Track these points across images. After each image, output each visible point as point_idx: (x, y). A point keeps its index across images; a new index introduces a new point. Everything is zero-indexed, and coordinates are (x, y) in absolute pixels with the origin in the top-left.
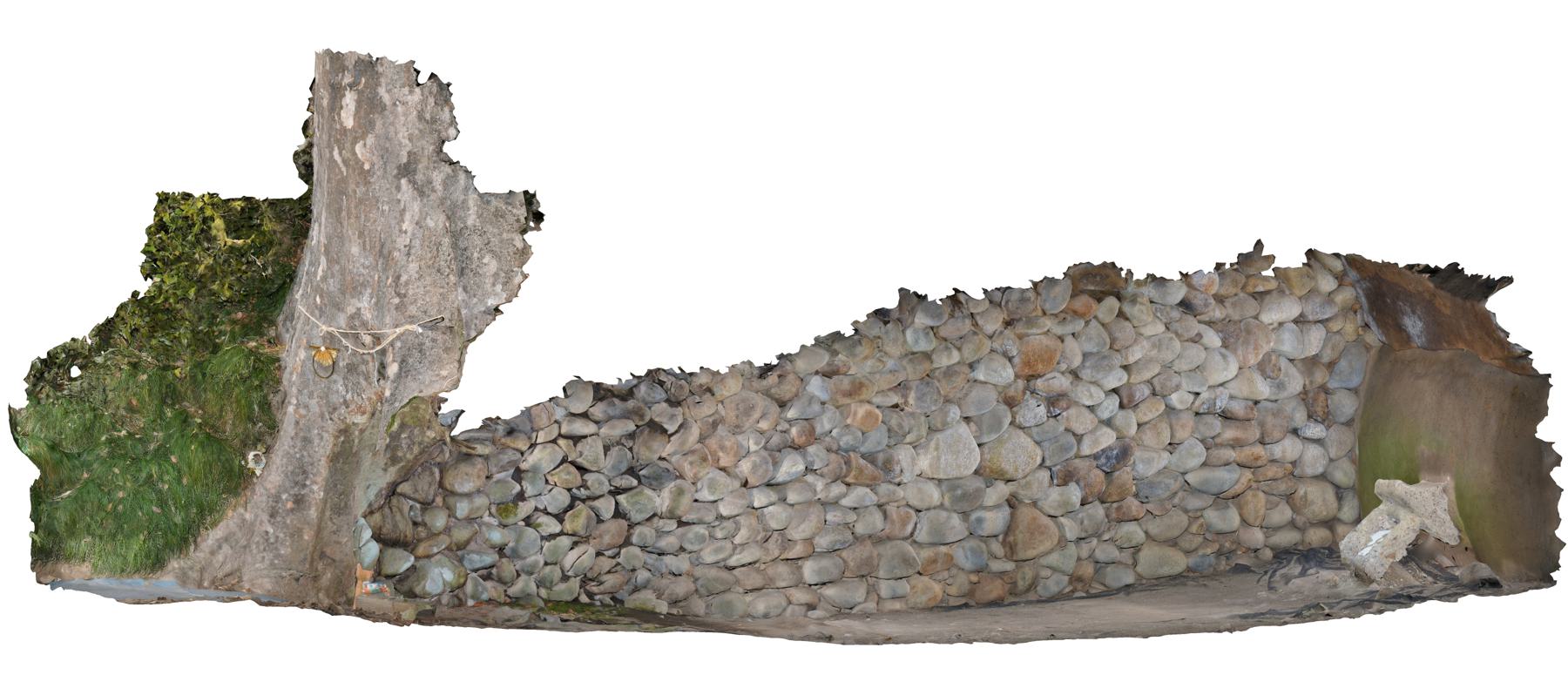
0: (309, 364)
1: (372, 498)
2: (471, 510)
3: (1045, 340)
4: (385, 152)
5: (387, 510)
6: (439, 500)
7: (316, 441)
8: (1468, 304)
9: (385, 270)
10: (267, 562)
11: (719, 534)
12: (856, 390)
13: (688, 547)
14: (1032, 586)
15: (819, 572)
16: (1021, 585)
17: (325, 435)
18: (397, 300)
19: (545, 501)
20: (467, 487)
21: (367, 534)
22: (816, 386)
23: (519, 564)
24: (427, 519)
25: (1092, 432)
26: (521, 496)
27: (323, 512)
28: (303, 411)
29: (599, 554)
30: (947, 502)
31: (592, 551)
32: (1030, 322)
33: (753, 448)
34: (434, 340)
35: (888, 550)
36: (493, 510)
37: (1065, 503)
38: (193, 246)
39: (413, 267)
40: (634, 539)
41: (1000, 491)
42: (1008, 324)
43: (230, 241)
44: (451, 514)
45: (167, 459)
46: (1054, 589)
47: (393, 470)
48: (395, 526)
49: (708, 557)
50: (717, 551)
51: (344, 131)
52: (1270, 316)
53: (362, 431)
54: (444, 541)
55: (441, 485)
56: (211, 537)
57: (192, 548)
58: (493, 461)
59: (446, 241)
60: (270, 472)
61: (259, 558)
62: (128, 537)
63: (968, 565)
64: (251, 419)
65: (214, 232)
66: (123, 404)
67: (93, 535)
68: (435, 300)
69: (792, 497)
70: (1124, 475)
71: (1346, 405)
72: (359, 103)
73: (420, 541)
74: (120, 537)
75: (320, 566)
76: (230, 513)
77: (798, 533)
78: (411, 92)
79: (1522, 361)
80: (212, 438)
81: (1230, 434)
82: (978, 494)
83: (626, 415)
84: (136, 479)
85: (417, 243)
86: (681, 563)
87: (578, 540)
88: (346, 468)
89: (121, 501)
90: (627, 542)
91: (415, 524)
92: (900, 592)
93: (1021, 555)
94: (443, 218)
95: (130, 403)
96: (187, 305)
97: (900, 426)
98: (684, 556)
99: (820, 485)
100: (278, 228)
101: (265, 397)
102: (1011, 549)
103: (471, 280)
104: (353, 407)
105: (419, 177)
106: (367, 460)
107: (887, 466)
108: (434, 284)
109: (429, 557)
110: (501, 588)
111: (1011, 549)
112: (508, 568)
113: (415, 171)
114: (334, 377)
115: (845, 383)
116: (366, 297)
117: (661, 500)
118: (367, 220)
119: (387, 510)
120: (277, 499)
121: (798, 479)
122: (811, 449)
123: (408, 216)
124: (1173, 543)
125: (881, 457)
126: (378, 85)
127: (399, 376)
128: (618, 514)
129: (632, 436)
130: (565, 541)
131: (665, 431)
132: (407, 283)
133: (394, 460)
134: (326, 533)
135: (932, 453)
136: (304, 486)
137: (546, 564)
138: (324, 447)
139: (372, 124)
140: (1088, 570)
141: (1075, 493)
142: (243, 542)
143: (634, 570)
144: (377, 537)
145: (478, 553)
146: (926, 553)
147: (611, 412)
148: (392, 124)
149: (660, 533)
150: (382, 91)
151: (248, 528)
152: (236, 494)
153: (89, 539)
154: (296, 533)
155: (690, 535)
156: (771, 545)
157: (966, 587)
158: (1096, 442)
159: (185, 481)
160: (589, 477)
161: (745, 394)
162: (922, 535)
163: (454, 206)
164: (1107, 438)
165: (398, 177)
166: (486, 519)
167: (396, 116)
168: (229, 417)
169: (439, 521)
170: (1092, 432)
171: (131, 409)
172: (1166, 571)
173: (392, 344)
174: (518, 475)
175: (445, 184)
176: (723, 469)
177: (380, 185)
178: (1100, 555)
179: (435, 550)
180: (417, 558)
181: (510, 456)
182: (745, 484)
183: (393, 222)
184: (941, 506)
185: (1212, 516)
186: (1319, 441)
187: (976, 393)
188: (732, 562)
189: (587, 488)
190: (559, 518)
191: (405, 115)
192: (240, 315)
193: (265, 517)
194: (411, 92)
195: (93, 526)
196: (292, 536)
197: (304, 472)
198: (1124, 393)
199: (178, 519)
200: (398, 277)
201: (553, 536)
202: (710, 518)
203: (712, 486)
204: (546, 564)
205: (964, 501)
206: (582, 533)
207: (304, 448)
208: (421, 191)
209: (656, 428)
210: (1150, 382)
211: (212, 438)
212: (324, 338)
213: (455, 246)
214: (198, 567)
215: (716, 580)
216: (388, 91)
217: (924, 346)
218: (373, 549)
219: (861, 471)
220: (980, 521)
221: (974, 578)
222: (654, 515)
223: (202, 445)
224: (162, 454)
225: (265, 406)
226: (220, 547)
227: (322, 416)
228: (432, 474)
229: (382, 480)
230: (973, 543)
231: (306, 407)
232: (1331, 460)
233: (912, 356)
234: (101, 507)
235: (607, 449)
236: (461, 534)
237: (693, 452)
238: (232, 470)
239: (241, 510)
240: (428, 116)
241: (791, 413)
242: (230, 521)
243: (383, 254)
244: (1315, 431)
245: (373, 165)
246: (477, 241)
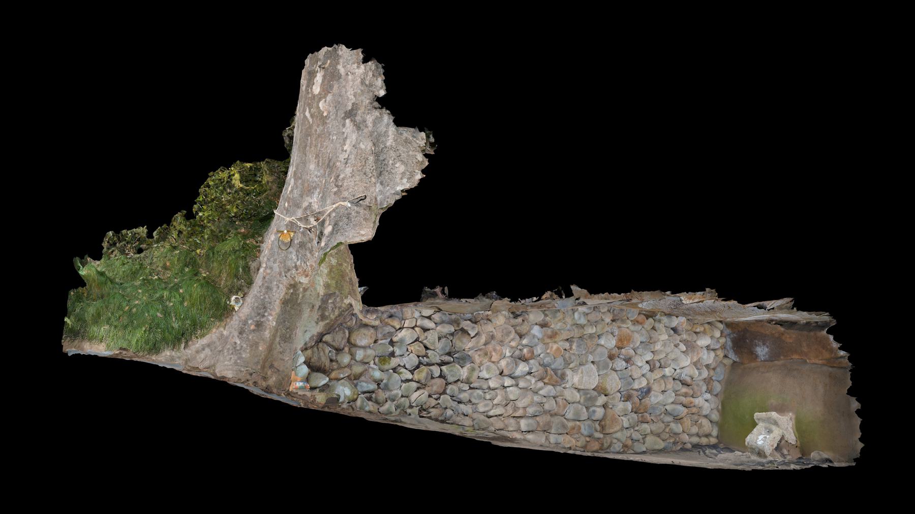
0: (276, 243)
1: (307, 339)
2: (365, 356)
4: (337, 104)
5: (315, 349)
6: (346, 349)
7: (275, 289)
8: (812, 334)
9: (330, 174)
10: (233, 361)
11: (488, 397)
12: (553, 336)
13: (473, 400)
14: (610, 446)
15: (528, 425)
16: (606, 445)
17: (281, 286)
18: (336, 189)
19: (405, 361)
20: (363, 342)
21: (302, 359)
22: (536, 330)
23: (388, 394)
24: (339, 358)
25: (639, 378)
26: (392, 354)
27: (274, 336)
28: (268, 271)
29: (430, 396)
30: (582, 401)
31: (426, 393)
32: (623, 321)
33: (508, 354)
34: (358, 212)
35: (556, 420)
36: (377, 360)
37: (625, 410)
38: (222, 193)
39: (348, 170)
40: (448, 391)
41: (602, 400)
42: (613, 321)
43: (241, 186)
44: (353, 355)
45: (177, 290)
46: (618, 449)
47: (322, 324)
48: (319, 358)
49: (481, 408)
50: (486, 405)
51: (314, 96)
53: (305, 290)
54: (347, 372)
55: (349, 341)
56: (198, 343)
57: (183, 345)
58: (380, 330)
59: (371, 158)
60: (243, 307)
61: (228, 358)
62: (135, 329)
63: (586, 433)
64: (236, 276)
65: (233, 182)
66: (161, 265)
67: (111, 325)
68: (361, 189)
69: (522, 384)
70: (646, 401)
71: (718, 387)
72: (324, 77)
73: (333, 370)
74: (130, 329)
75: (269, 373)
76: (214, 330)
77: (520, 404)
78: (358, 67)
80: (210, 283)
81: (684, 390)
82: (595, 399)
83: (451, 322)
84: (151, 296)
85: (352, 157)
87: (421, 386)
88: (293, 312)
89: (135, 306)
90: (444, 393)
91: (331, 361)
93: (607, 431)
94: (370, 144)
95: (165, 264)
96: (213, 224)
97: (570, 358)
98: (469, 406)
99: (533, 381)
100: (270, 179)
101: (247, 263)
102: (603, 428)
103: (386, 176)
104: (300, 270)
105: (358, 118)
106: (306, 313)
107: (563, 377)
108: (361, 180)
109: (338, 380)
110: (376, 406)
111: (603, 428)
112: (382, 395)
113: (355, 115)
114: (291, 249)
115: (549, 331)
116: (316, 195)
117: (464, 373)
118: (322, 147)
119: (315, 349)
120: (245, 323)
121: (523, 377)
122: (531, 362)
123: (348, 142)
125: (559, 372)
126: (338, 63)
127: (332, 233)
128: (442, 376)
129: (452, 334)
130: (414, 385)
131: (469, 334)
132: (343, 179)
133: (323, 317)
134: (275, 352)
135: (579, 375)
136: (264, 316)
137: (402, 396)
138: (279, 293)
139: (331, 87)
140: (629, 442)
141: (629, 406)
142: (220, 348)
143: (446, 408)
144: (307, 363)
145: (366, 382)
146: (570, 424)
147: (444, 318)
148: (344, 87)
149: (461, 391)
150: (340, 67)
151: (224, 339)
152: (221, 320)
153: (107, 327)
154: (255, 345)
155: (475, 394)
156: (509, 408)
157: (584, 443)
158: (640, 383)
159: (185, 304)
160: (430, 352)
161: (506, 326)
162: (570, 415)
163: (379, 135)
164: (644, 383)
165: (344, 119)
166: (372, 365)
167: (347, 81)
168: (224, 276)
169: (346, 359)
170: (639, 378)
171: (165, 268)
172: (657, 447)
173: (329, 215)
174: (392, 343)
175: (375, 123)
176: (493, 362)
177: (332, 124)
179: (342, 376)
180: (330, 380)
181: (388, 329)
182: (501, 373)
183: (338, 145)
185: (673, 425)
187: (599, 349)
188: (491, 413)
189: (428, 357)
190: (412, 372)
191: (353, 81)
192: (243, 230)
193: (236, 334)
194: (358, 67)
195: (113, 319)
196: (251, 346)
197: (265, 308)
198: (651, 363)
199: (176, 325)
200: (338, 176)
201: (408, 381)
202: (485, 387)
203: (488, 369)
204: (402, 396)
206: (423, 381)
207: (267, 293)
208: (358, 127)
209: (464, 331)
211: (210, 283)
212: (287, 225)
213: (376, 161)
214: (185, 358)
215: (484, 421)
216: (344, 67)
217: (583, 321)
218: (305, 370)
221: (588, 439)
222: (458, 380)
223: (202, 286)
224: (176, 287)
225: (247, 269)
226: (203, 349)
227: (280, 274)
228: (344, 333)
229: (316, 329)
230: (589, 422)
231: (271, 268)
234: (120, 308)
235: (439, 339)
236: (358, 369)
237: (480, 350)
238: (219, 304)
239: (222, 329)
240: (367, 82)
241: (525, 342)
242: (213, 335)
243: (330, 166)
245: (329, 112)
246: (392, 154)
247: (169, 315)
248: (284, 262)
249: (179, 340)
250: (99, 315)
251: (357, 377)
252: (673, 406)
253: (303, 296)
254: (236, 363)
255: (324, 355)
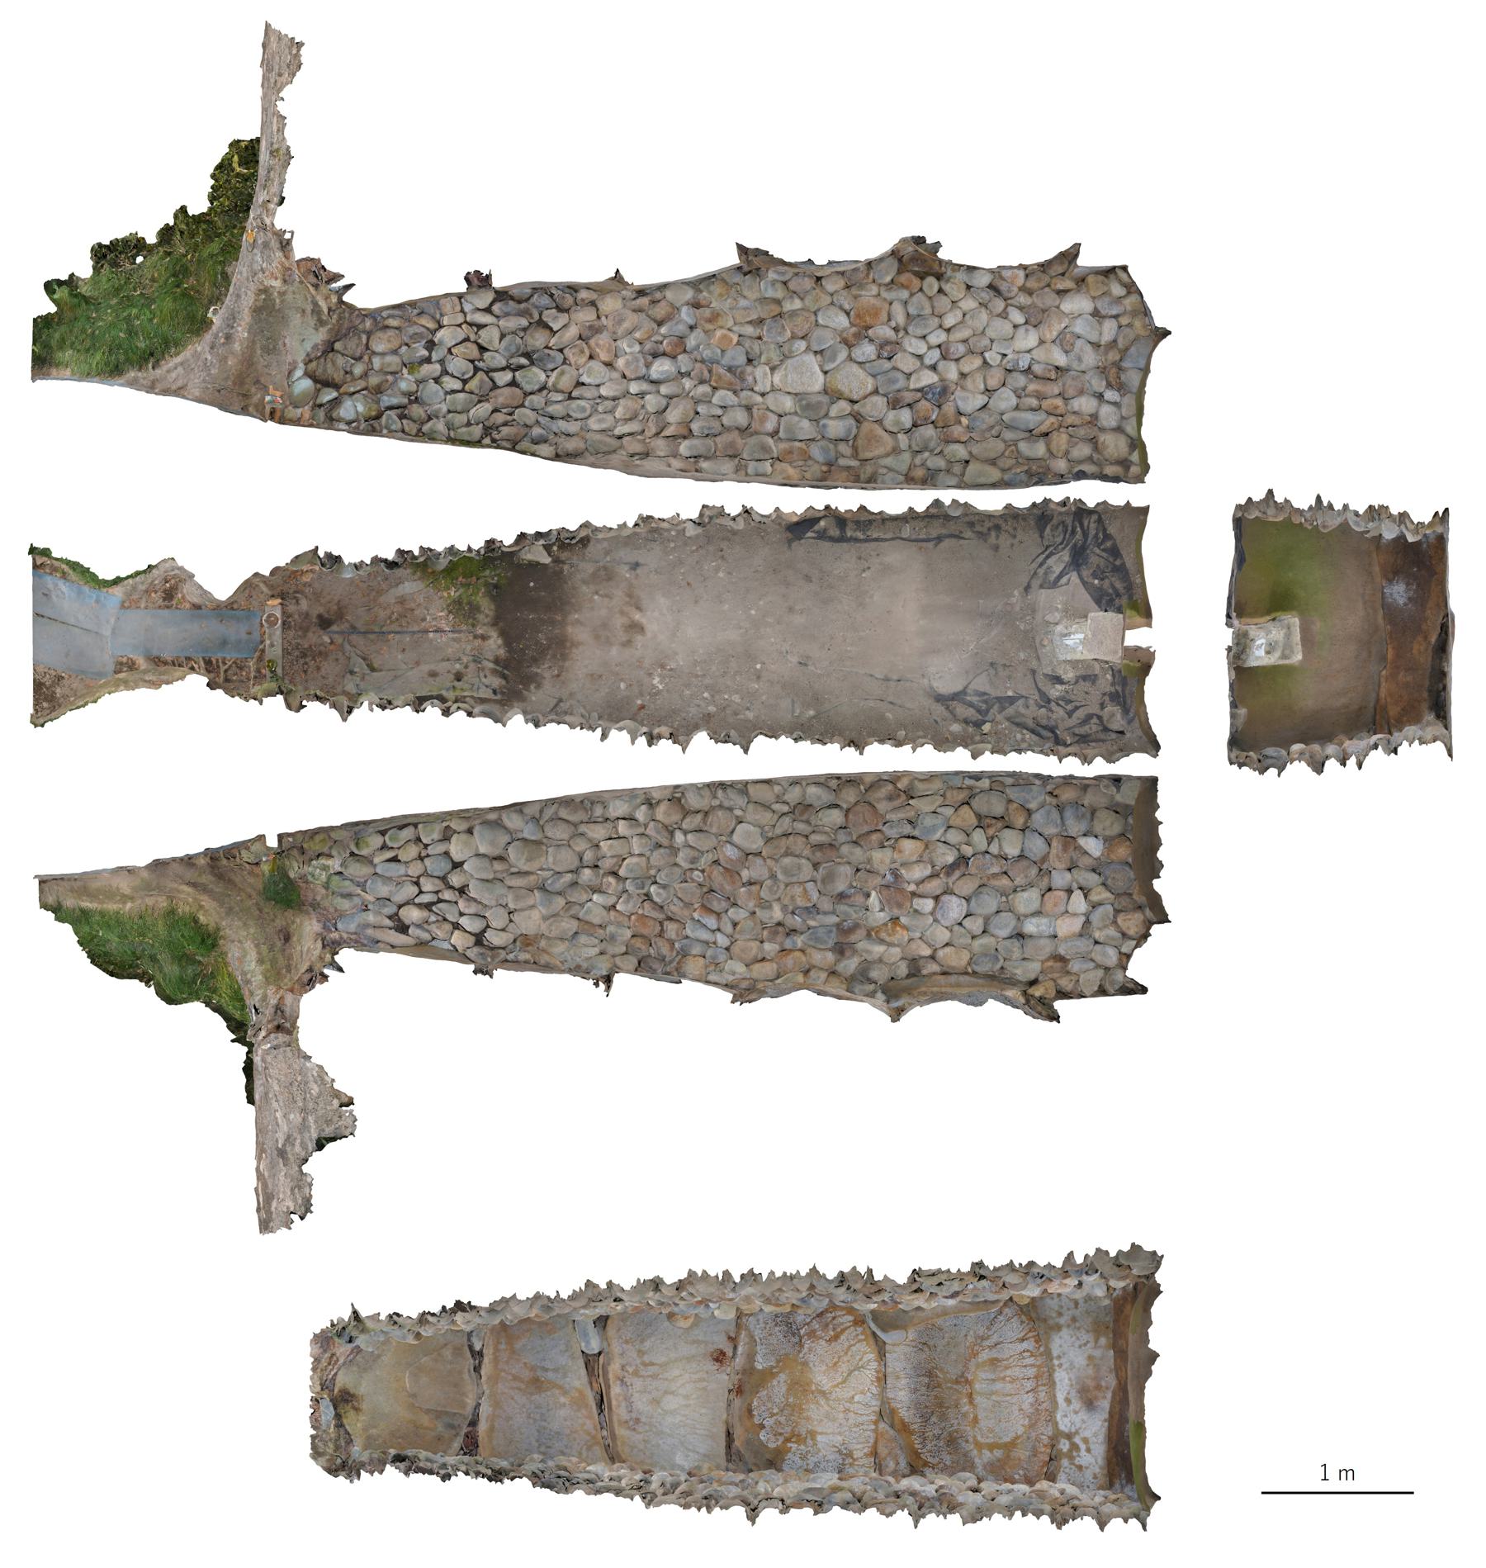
3: (873, 301)
15: (690, 448)
22: (686, 315)
32: (861, 286)
42: (848, 287)
48: (325, 370)
50: (600, 421)
52: (1068, 305)
75: (253, 390)
79: (1148, 1500)
83: (521, 314)
86: (573, 427)
92: (761, 471)
106: (296, 319)
115: (707, 313)
120: (216, 336)
124: (993, 462)
129: (525, 330)
131: (551, 329)
133: (321, 323)
137: (449, 411)
146: (783, 446)
152: (198, 335)
154: (224, 360)
158: (918, 379)
160: (486, 355)
178: (929, 464)
184: (796, 413)
186: (1115, 404)
187: (818, 332)
201: (454, 392)
204: (449, 411)
205: (808, 407)
209: (542, 324)
210: (965, 341)
215: (600, 442)
219: (720, 377)
220: (824, 426)
230: (823, 443)
232: (1123, 418)
233: (763, 300)
234: (83, 331)
235: (503, 336)
241: (663, 330)
244: (1110, 395)
247: (136, 334)
248: (251, 266)
249: (146, 360)
250: (63, 340)
251: (378, 390)
252: (1017, 414)
253: (282, 302)
254: (204, 381)
255: (335, 367)
